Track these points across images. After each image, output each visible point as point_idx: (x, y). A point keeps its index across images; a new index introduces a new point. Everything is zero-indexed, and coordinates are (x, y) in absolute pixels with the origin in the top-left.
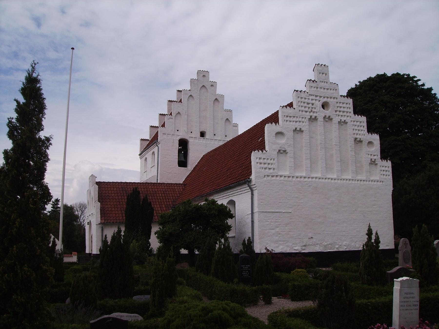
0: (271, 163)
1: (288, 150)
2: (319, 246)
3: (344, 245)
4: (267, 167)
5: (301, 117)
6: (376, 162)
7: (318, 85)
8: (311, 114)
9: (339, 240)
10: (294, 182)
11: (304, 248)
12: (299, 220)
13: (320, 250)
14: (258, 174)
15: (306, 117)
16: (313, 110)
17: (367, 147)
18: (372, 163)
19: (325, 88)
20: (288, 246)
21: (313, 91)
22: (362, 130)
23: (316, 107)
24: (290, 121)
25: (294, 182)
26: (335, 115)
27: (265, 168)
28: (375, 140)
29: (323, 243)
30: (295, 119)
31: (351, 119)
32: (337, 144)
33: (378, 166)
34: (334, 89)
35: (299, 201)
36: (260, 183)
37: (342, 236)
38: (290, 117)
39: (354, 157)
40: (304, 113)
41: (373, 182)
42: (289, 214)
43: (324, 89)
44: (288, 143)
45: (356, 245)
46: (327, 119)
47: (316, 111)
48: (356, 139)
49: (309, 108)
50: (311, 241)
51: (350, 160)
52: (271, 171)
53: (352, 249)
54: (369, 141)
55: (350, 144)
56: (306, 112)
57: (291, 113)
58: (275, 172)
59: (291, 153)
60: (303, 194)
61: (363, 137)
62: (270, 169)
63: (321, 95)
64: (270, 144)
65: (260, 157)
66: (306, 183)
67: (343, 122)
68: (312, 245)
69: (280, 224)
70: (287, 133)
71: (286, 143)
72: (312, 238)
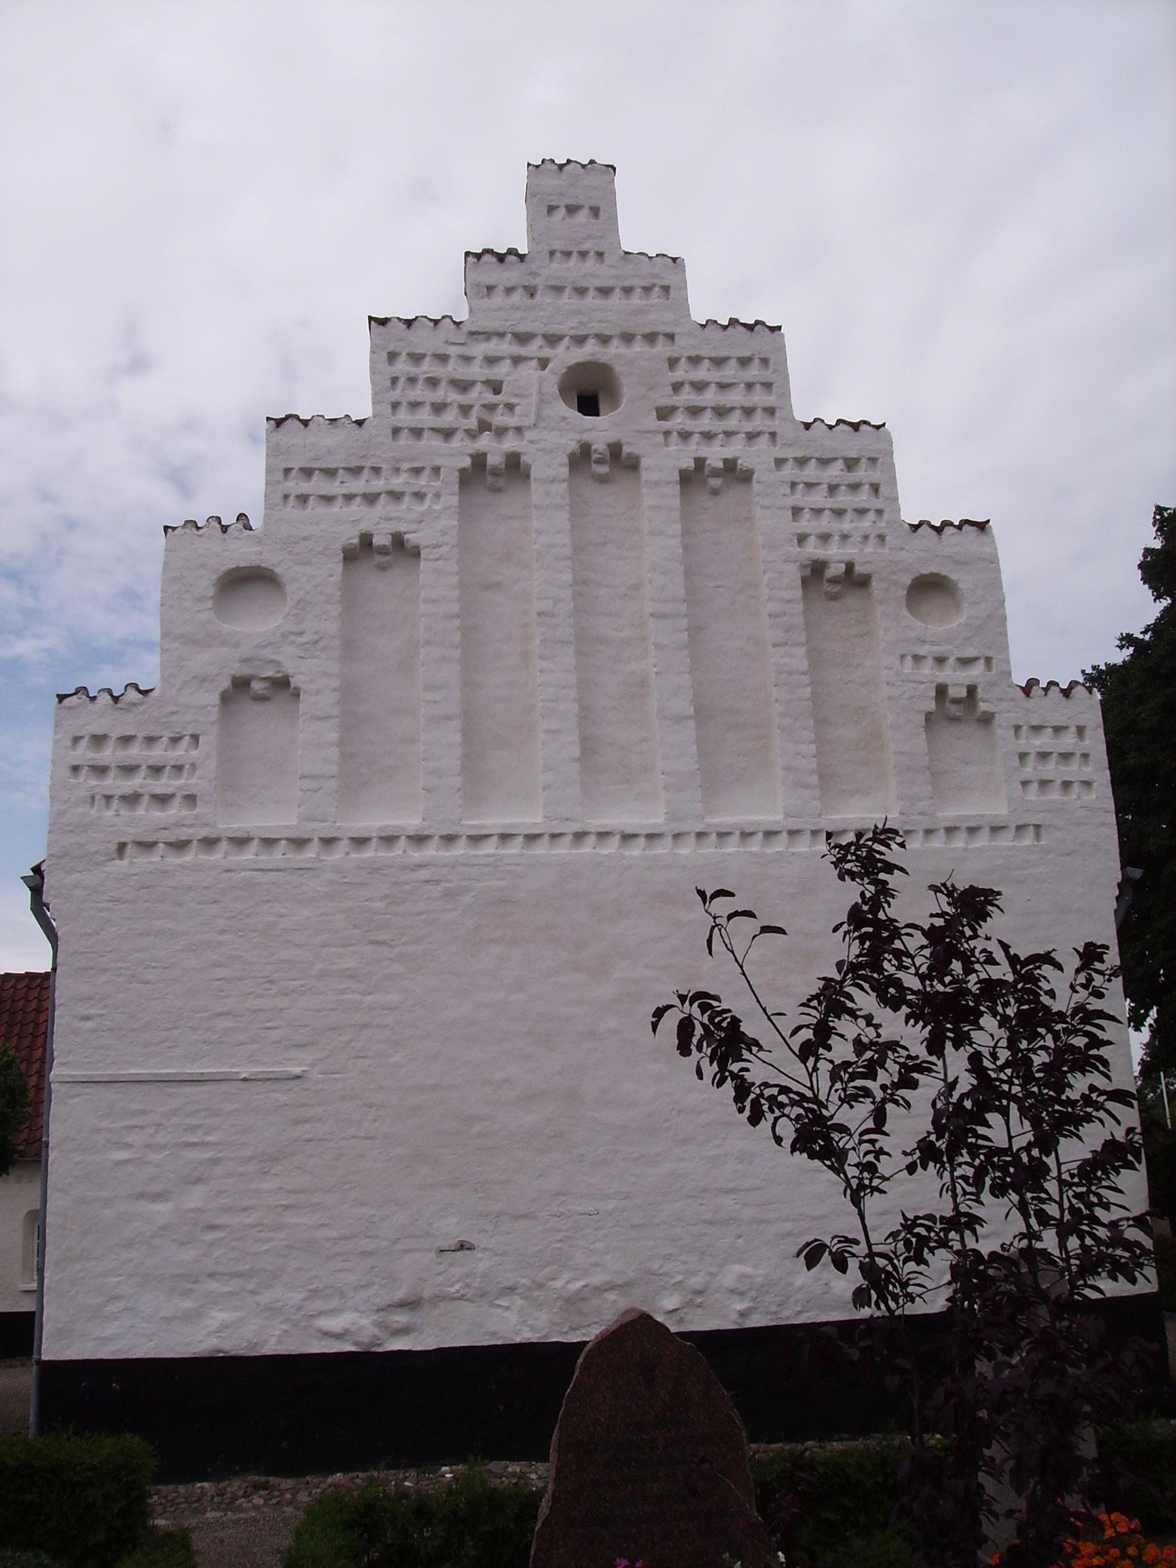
0: (173, 763)
1: (301, 673)
2: (519, 1302)
3: (733, 1291)
4: (141, 791)
5: (405, 466)
6: (983, 706)
7: (533, 274)
8: (485, 442)
9: (683, 1258)
10: (334, 876)
11: (401, 1318)
12: (365, 1124)
13: (533, 1329)
14: (74, 839)
15: (438, 462)
16: (499, 419)
17: (908, 614)
18: (953, 709)
19: (583, 284)
20: (271, 1310)
21: (500, 309)
22: (862, 512)
23: (514, 400)
24: (328, 499)
25: (334, 876)
26: (657, 432)
27: (132, 799)
28: (960, 563)
29: (559, 1284)
30: (358, 485)
31: (779, 452)
32: (667, 608)
33: (1002, 731)
34: (654, 285)
35: (368, 999)
36: (79, 893)
37: (711, 1223)
38: (330, 473)
39: (806, 679)
40: (431, 442)
41: (963, 835)
42: (289, 1090)
43: (582, 292)
44: (300, 634)
45: (833, 1284)
46: (600, 462)
47: (518, 425)
48: (816, 571)
49: (465, 410)
50: (457, 1271)
51: (776, 705)
52: (174, 811)
53: (799, 1313)
54: (922, 576)
55: (770, 599)
56: (447, 434)
57: (329, 451)
58: (197, 817)
59: (318, 692)
60: (396, 950)
61: (869, 550)
62: (163, 800)
63: (554, 329)
64: (176, 645)
65: (99, 732)
66: (423, 874)
67: (716, 473)
68: (462, 1298)
69: (216, 1162)
70: (296, 568)
71: (284, 636)
72: (462, 1246)
